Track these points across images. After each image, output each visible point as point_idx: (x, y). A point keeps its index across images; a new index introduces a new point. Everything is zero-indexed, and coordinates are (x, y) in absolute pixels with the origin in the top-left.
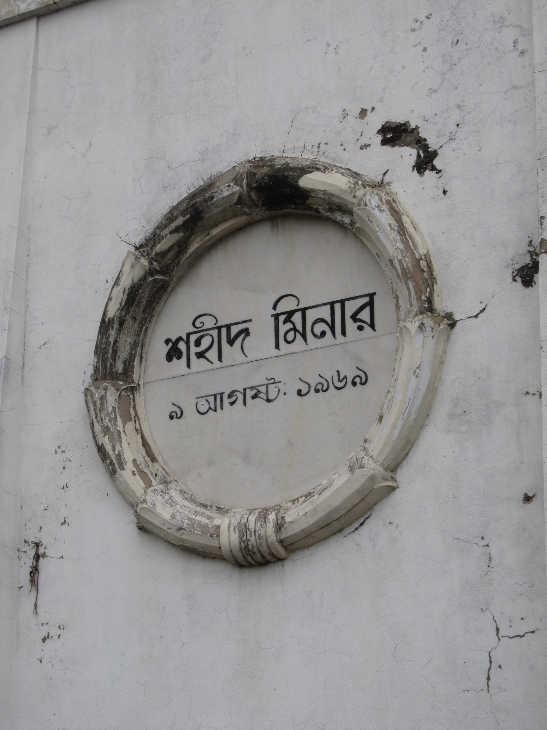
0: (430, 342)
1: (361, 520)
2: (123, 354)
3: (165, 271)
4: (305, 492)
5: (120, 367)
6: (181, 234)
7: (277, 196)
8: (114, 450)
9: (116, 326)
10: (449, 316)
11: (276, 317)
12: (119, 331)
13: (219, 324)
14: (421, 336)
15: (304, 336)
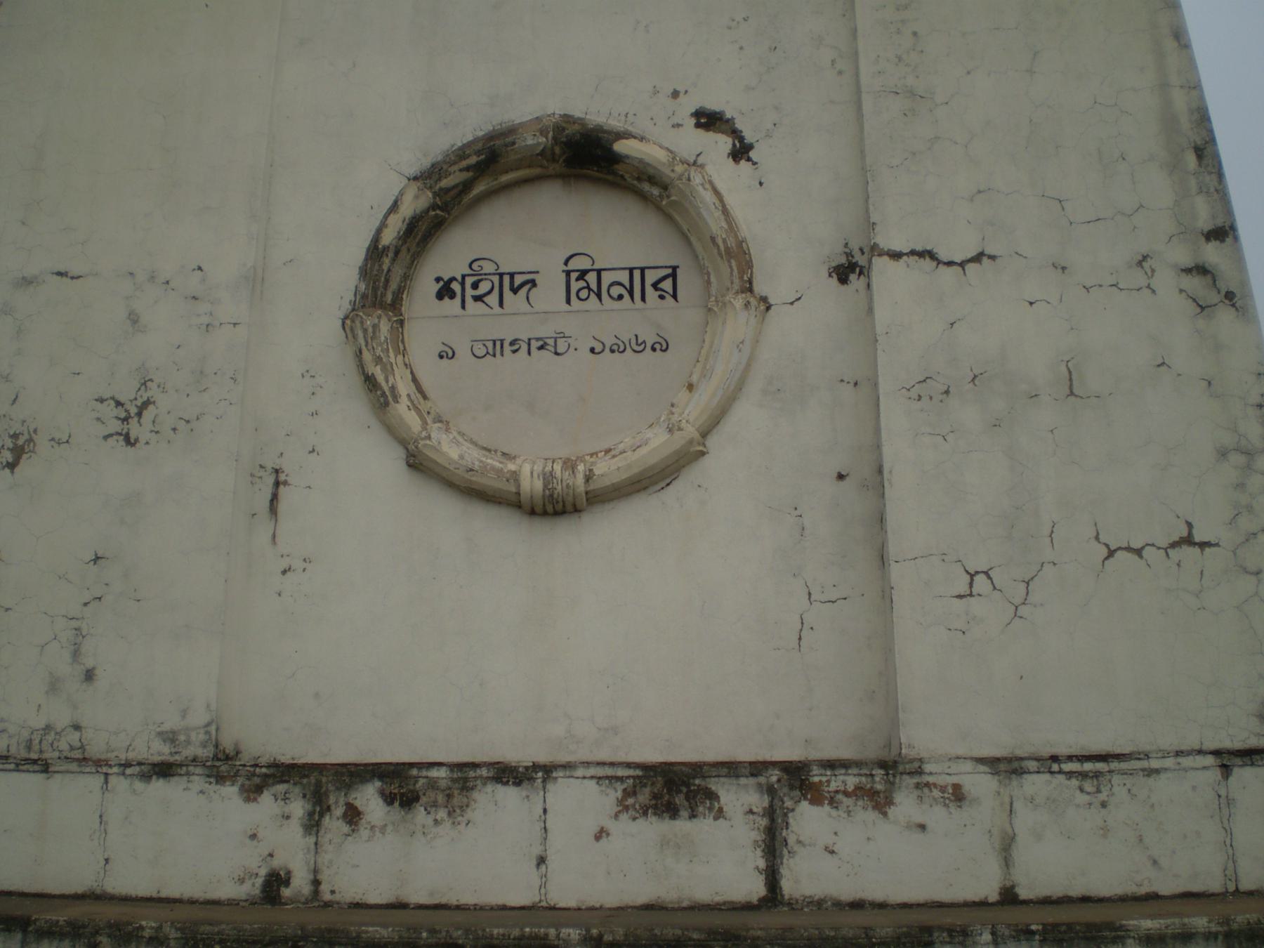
0: (753, 321)
1: (668, 481)
2: (393, 286)
3: (445, 207)
4: (606, 447)
5: (389, 298)
6: (471, 174)
7: (585, 156)
8: (387, 382)
9: (391, 255)
10: (764, 299)
11: (568, 273)
12: (394, 260)
13: (500, 271)
14: (746, 313)
15: (599, 296)
